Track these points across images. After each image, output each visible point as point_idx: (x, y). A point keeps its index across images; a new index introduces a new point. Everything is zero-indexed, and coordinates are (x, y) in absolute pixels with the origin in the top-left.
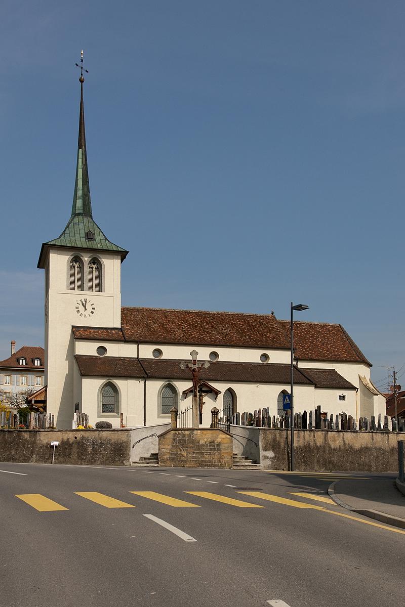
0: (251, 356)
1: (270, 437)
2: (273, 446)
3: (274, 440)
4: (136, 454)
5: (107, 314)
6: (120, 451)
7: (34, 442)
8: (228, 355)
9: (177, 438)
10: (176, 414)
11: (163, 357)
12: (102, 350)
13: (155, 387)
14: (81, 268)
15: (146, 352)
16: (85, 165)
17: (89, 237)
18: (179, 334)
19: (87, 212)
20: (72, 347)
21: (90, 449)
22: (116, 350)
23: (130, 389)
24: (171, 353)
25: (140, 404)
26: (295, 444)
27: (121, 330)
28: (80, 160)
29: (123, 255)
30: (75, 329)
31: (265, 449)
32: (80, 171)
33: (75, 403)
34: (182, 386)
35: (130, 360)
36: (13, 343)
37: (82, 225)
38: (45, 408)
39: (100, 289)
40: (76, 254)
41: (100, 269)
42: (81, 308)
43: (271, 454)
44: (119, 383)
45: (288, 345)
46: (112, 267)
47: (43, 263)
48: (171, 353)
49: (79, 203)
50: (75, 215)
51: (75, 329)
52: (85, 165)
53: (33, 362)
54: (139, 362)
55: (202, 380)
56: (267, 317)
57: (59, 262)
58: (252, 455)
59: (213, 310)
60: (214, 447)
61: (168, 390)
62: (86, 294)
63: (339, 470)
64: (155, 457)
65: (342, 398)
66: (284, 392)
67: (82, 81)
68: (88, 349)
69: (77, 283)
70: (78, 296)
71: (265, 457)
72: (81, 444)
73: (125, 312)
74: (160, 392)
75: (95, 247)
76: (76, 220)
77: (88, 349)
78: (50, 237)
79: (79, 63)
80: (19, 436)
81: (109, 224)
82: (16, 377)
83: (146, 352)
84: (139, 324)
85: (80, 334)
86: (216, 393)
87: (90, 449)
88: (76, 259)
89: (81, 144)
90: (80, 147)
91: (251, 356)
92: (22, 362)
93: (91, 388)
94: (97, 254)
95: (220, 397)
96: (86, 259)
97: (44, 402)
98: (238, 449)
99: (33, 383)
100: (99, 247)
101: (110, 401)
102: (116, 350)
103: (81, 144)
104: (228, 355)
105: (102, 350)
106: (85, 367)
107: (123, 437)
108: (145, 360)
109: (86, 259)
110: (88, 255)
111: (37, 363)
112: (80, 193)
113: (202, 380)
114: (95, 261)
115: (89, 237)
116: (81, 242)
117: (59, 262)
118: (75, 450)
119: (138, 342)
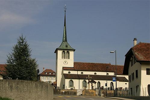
0: (104, 74)
1: (103, 91)
2: (103, 93)
3: (104, 92)
4: (78, 94)
5: (70, 63)
6: (75, 93)
7: (60, 92)
8: (99, 73)
9: (86, 92)
10: (86, 87)
11: (83, 74)
12: (69, 72)
13: (81, 81)
14: (65, 53)
15: (79, 73)
16: (66, 30)
17: (67, 46)
18: (87, 69)
19: (66, 40)
20: (63, 72)
21: (70, 93)
22: (73, 72)
23: (76, 81)
24: (85, 73)
25: (78, 85)
26: (108, 93)
27: (74, 68)
28: (65, 31)
29: (74, 50)
30: (63, 68)
31: (102, 94)
32: (65, 31)
33: (63, 84)
34: (87, 81)
35: (76, 75)
36: (44, 68)
37: (65, 44)
38: (56, 85)
39: (69, 58)
40: (64, 50)
41: (69, 54)
42: (65, 63)
43: (103, 94)
44: (73, 80)
45: (113, 71)
46: (72, 53)
47: (56, 52)
48: (85, 73)
49: (64, 38)
50: (63, 41)
51: (63, 68)
52: (66, 30)
53: (49, 73)
54: (78, 75)
55: (92, 79)
56: (108, 64)
57: (60, 53)
58: (99, 95)
59: (95, 62)
60: (92, 93)
61: (84, 82)
62: (66, 60)
63: (106, 96)
64: (81, 95)
65: (126, 84)
66: (112, 82)
67: (65, 11)
68: (66, 72)
69: (64, 57)
70: (64, 60)
71: (102, 95)
72: (68, 92)
73: (75, 63)
74: (82, 82)
75: (68, 49)
76: (63, 42)
77: (66, 72)
78: (58, 47)
79: (65, 7)
80: (57, 90)
81: (71, 44)
82: (45, 77)
83: (79, 73)
84: (78, 66)
85: (64, 69)
86: (96, 82)
87: (70, 93)
88: (64, 52)
89: (65, 25)
90: (65, 26)
91: (104, 74)
92: (46, 73)
93: (67, 81)
94: (68, 51)
95: (97, 83)
96: (66, 52)
97: (56, 84)
98: (97, 93)
99: (53, 80)
100: (69, 49)
101: (71, 84)
102: (73, 72)
103: (65, 25)
104: (99, 73)
105: (69, 72)
106: (66, 76)
107: (76, 91)
108: (79, 75)
109: (66, 52)
110: (66, 51)
111: (54, 74)
112: (64, 36)
113: (92, 79)
114: (68, 52)
115: (67, 46)
116: (65, 48)
117: (60, 53)
118: (67, 93)
119: (78, 71)
